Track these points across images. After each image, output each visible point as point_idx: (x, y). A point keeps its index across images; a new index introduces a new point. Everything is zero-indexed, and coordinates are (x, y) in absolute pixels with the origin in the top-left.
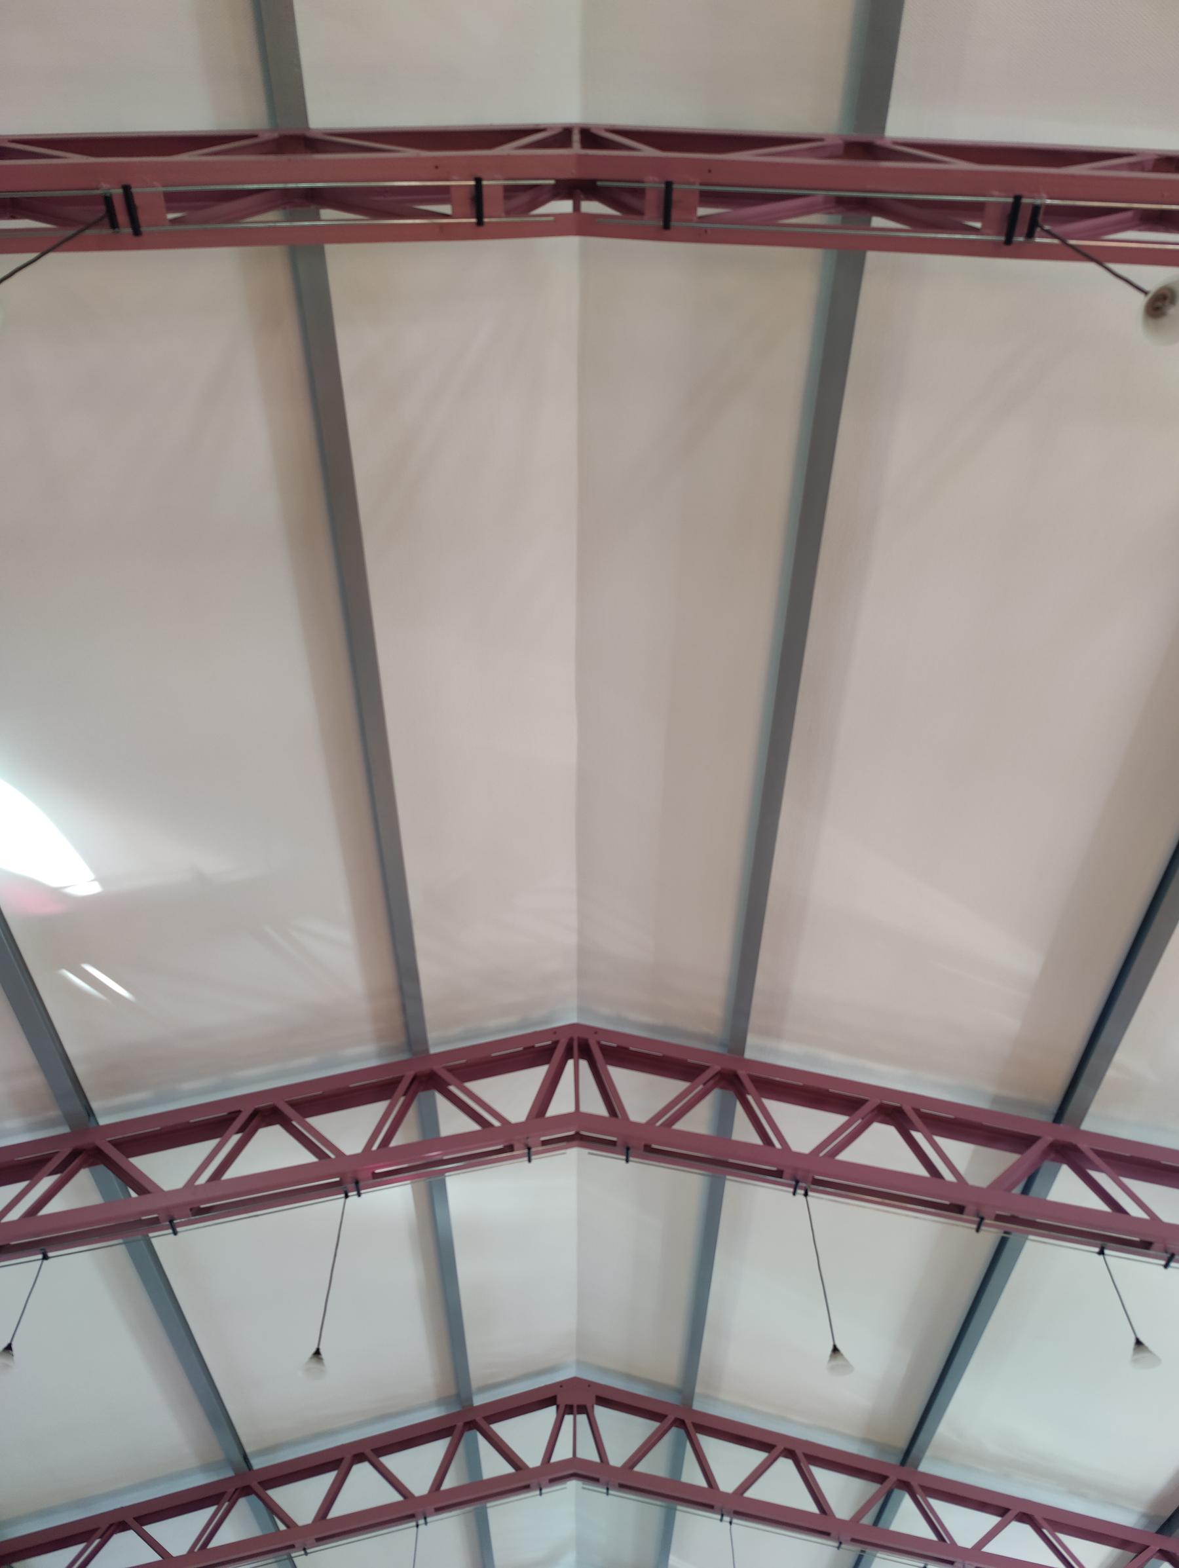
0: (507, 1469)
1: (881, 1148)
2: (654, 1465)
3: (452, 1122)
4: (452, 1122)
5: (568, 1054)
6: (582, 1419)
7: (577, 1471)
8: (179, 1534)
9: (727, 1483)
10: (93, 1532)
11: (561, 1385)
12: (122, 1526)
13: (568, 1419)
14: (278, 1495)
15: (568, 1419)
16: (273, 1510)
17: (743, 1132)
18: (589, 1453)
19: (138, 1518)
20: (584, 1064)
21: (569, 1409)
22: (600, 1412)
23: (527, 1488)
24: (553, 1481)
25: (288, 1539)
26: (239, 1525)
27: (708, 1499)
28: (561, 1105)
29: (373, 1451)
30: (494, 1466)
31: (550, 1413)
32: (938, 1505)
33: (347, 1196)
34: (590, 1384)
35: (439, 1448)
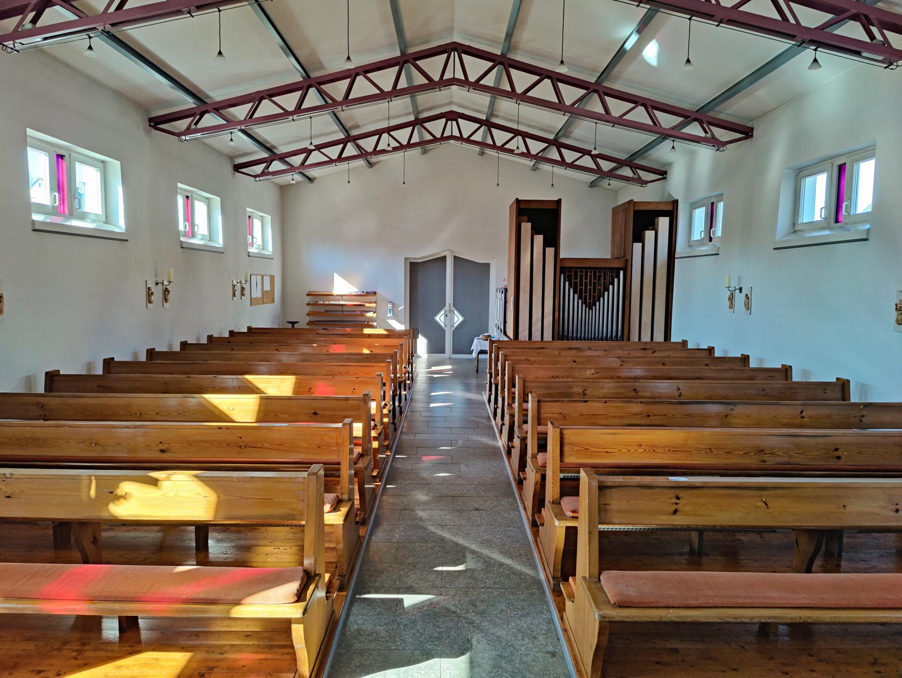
2: (478, 137)
6: (454, 123)
7: (454, 81)
13: (449, 122)
15: (449, 122)
16: (359, 147)
18: (456, 133)
22: (459, 120)
31: (444, 120)
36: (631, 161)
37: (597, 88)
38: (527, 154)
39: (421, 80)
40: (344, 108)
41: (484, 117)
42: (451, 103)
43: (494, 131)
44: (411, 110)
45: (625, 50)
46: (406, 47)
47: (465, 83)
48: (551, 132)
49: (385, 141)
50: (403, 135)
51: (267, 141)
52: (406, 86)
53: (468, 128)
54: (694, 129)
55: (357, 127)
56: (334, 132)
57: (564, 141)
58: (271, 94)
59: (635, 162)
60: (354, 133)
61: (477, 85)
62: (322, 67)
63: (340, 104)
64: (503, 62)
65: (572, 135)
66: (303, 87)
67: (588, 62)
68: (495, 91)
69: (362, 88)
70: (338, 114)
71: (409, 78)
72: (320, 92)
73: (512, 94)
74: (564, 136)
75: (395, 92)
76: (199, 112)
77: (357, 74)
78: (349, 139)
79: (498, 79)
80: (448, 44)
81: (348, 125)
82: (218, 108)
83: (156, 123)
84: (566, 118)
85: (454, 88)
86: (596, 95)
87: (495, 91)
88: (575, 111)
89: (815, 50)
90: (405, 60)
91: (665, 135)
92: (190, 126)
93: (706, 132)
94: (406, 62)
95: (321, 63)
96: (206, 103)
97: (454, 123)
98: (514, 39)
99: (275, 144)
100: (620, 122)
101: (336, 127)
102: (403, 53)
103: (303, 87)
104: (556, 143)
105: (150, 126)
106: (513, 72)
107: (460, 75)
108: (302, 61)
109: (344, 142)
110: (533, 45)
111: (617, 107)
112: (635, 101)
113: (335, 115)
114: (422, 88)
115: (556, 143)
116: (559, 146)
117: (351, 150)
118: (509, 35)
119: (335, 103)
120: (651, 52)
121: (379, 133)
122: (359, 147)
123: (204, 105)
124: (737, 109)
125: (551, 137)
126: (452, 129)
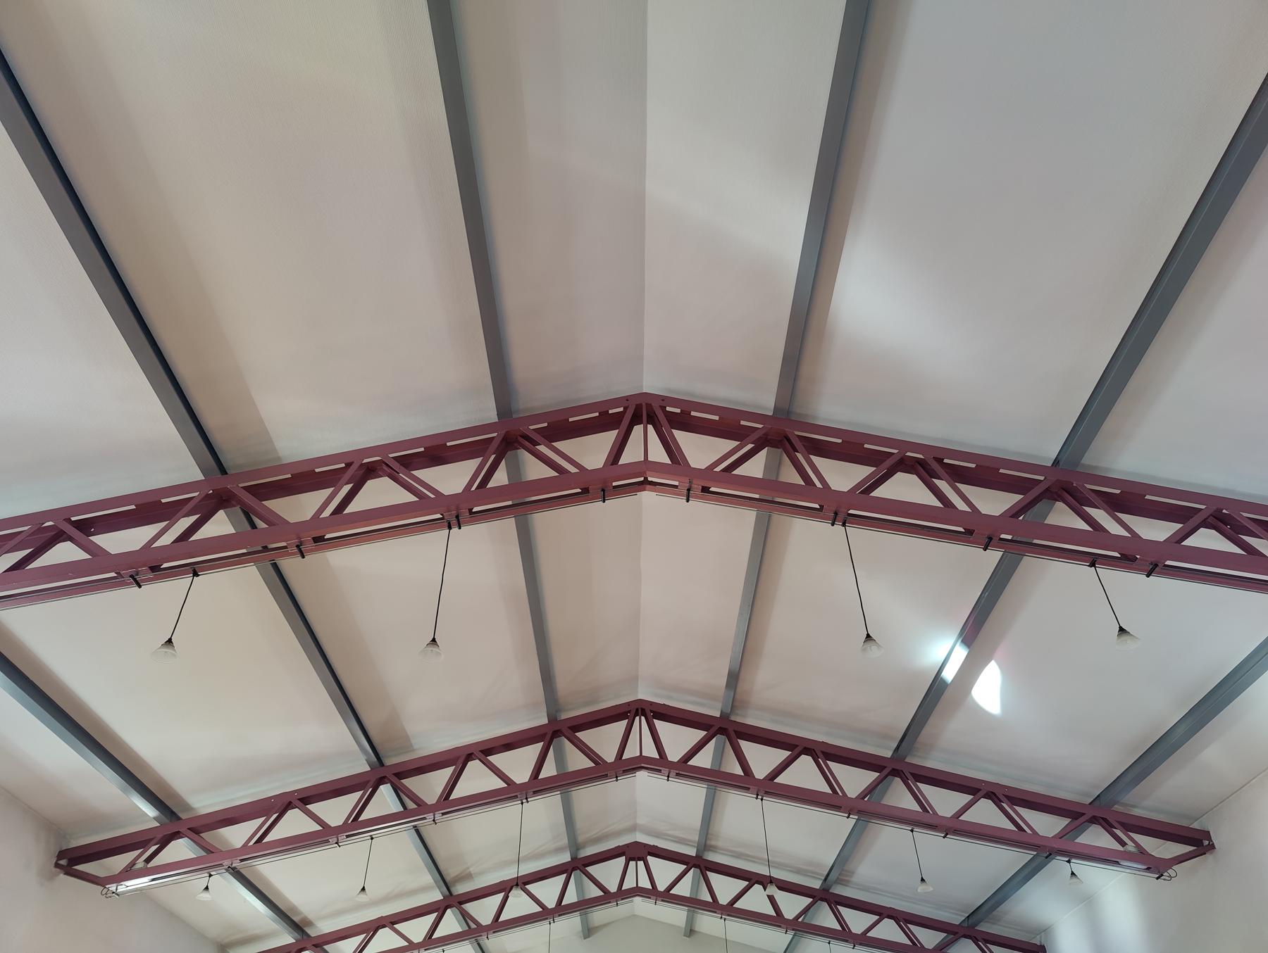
0: (589, 764)
1: (804, 774)
2: (683, 889)
3: (535, 470)
4: (535, 470)
5: (636, 420)
6: (641, 863)
7: (637, 891)
8: (417, 930)
9: (723, 900)
10: (371, 929)
11: (628, 845)
12: (384, 926)
14: (469, 907)
15: (632, 864)
16: (465, 916)
17: (790, 476)
18: (645, 883)
19: (391, 921)
20: (650, 427)
21: (633, 859)
23: (605, 777)
24: (625, 772)
25: (473, 931)
26: (451, 923)
27: (745, 781)
28: (631, 455)
29: (522, 883)
30: (578, 762)
31: (621, 860)
32: (926, 789)
33: (450, 528)
34: (645, 845)
35: (534, 750)
36: (972, 927)
37: (897, 767)
38: (777, 920)
39: (583, 763)
40: (438, 816)
41: (692, 852)
42: (633, 829)
43: (712, 876)
44: (565, 841)
45: (944, 682)
46: (558, 711)
47: (652, 893)
48: (813, 875)
49: (519, 904)
50: (548, 891)
51: (294, 909)
52: (575, 900)
53: (665, 872)
54: (1096, 837)
55: (468, 876)
56: (424, 889)
57: (839, 890)
58: (304, 799)
59: (980, 928)
60: (461, 889)
61: (667, 896)
62: (408, 747)
63: (433, 809)
64: (725, 729)
65: (855, 879)
66: (365, 784)
67: (878, 719)
68: (692, 903)
69: (476, 779)
70: (422, 830)
71: (560, 760)
72: (396, 790)
73: (714, 906)
74: (839, 881)
75: (561, 909)
76: (159, 836)
77: (470, 757)
78: (453, 901)
79: (695, 887)
80: (628, 704)
81: (451, 872)
82: (199, 828)
83: (72, 860)
84: (789, 936)
85: (637, 900)
86: (898, 780)
87: (692, 903)
88: (866, 810)
89: (1069, 862)
90: (557, 731)
91: (1045, 852)
92: (133, 863)
93: (1123, 844)
94: (556, 734)
95: (407, 738)
96: (179, 819)
97: (641, 863)
98: (742, 686)
99: (311, 917)
100: (954, 828)
101: (427, 878)
102: (552, 719)
103: (365, 784)
104: (824, 895)
105: (57, 865)
106: (745, 745)
107: (650, 751)
108: (372, 733)
109: (439, 909)
110: (775, 696)
111: (945, 802)
112: (882, 913)
113: (418, 832)
114: (596, 902)
115: (824, 895)
116: (836, 902)
117: (385, 800)
118: (734, 678)
119: (422, 808)
120: (989, 691)
121: (505, 888)
122: (465, 916)
123: (175, 821)
124: (1164, 794)
125: (816, 884)
126: (637, 876)
